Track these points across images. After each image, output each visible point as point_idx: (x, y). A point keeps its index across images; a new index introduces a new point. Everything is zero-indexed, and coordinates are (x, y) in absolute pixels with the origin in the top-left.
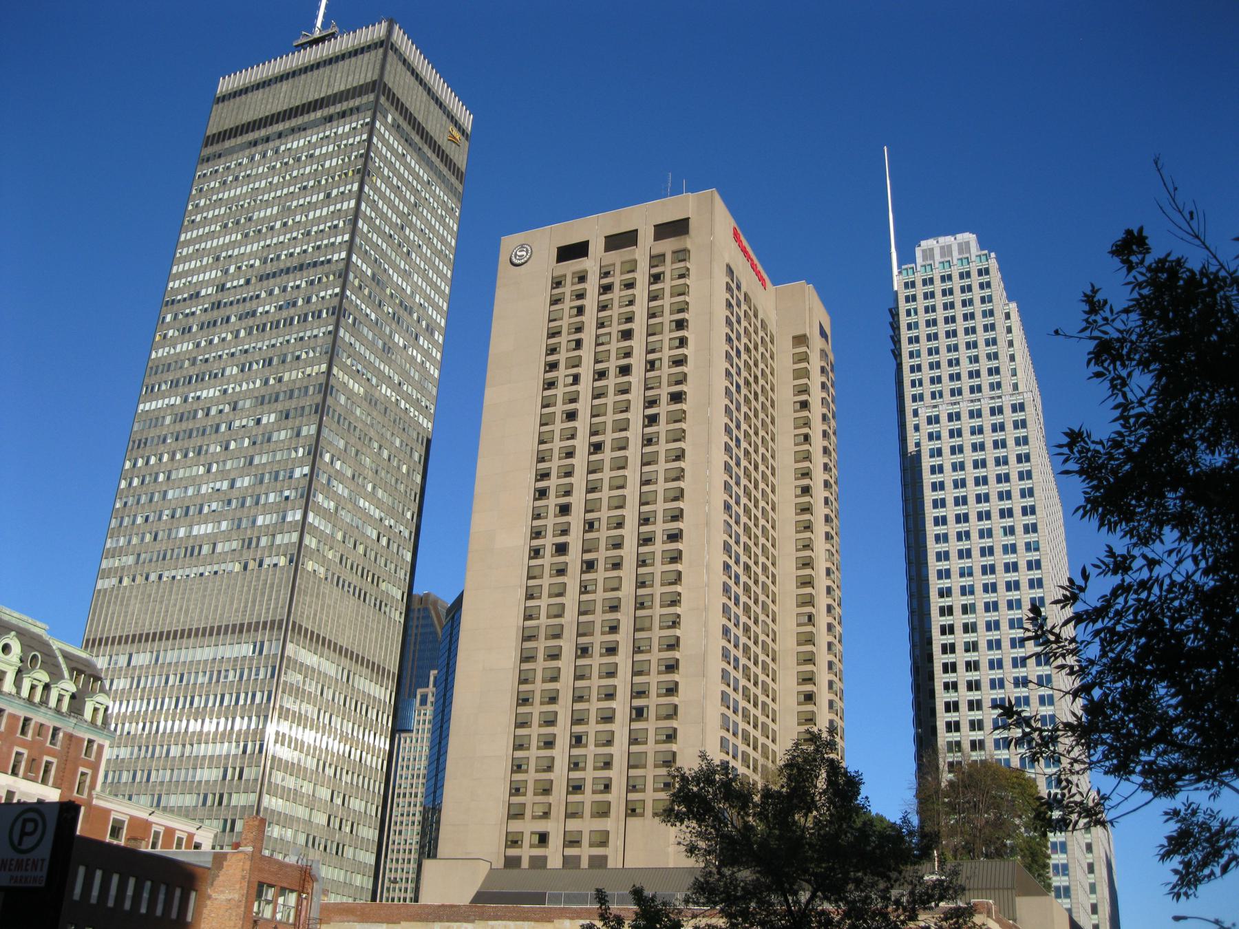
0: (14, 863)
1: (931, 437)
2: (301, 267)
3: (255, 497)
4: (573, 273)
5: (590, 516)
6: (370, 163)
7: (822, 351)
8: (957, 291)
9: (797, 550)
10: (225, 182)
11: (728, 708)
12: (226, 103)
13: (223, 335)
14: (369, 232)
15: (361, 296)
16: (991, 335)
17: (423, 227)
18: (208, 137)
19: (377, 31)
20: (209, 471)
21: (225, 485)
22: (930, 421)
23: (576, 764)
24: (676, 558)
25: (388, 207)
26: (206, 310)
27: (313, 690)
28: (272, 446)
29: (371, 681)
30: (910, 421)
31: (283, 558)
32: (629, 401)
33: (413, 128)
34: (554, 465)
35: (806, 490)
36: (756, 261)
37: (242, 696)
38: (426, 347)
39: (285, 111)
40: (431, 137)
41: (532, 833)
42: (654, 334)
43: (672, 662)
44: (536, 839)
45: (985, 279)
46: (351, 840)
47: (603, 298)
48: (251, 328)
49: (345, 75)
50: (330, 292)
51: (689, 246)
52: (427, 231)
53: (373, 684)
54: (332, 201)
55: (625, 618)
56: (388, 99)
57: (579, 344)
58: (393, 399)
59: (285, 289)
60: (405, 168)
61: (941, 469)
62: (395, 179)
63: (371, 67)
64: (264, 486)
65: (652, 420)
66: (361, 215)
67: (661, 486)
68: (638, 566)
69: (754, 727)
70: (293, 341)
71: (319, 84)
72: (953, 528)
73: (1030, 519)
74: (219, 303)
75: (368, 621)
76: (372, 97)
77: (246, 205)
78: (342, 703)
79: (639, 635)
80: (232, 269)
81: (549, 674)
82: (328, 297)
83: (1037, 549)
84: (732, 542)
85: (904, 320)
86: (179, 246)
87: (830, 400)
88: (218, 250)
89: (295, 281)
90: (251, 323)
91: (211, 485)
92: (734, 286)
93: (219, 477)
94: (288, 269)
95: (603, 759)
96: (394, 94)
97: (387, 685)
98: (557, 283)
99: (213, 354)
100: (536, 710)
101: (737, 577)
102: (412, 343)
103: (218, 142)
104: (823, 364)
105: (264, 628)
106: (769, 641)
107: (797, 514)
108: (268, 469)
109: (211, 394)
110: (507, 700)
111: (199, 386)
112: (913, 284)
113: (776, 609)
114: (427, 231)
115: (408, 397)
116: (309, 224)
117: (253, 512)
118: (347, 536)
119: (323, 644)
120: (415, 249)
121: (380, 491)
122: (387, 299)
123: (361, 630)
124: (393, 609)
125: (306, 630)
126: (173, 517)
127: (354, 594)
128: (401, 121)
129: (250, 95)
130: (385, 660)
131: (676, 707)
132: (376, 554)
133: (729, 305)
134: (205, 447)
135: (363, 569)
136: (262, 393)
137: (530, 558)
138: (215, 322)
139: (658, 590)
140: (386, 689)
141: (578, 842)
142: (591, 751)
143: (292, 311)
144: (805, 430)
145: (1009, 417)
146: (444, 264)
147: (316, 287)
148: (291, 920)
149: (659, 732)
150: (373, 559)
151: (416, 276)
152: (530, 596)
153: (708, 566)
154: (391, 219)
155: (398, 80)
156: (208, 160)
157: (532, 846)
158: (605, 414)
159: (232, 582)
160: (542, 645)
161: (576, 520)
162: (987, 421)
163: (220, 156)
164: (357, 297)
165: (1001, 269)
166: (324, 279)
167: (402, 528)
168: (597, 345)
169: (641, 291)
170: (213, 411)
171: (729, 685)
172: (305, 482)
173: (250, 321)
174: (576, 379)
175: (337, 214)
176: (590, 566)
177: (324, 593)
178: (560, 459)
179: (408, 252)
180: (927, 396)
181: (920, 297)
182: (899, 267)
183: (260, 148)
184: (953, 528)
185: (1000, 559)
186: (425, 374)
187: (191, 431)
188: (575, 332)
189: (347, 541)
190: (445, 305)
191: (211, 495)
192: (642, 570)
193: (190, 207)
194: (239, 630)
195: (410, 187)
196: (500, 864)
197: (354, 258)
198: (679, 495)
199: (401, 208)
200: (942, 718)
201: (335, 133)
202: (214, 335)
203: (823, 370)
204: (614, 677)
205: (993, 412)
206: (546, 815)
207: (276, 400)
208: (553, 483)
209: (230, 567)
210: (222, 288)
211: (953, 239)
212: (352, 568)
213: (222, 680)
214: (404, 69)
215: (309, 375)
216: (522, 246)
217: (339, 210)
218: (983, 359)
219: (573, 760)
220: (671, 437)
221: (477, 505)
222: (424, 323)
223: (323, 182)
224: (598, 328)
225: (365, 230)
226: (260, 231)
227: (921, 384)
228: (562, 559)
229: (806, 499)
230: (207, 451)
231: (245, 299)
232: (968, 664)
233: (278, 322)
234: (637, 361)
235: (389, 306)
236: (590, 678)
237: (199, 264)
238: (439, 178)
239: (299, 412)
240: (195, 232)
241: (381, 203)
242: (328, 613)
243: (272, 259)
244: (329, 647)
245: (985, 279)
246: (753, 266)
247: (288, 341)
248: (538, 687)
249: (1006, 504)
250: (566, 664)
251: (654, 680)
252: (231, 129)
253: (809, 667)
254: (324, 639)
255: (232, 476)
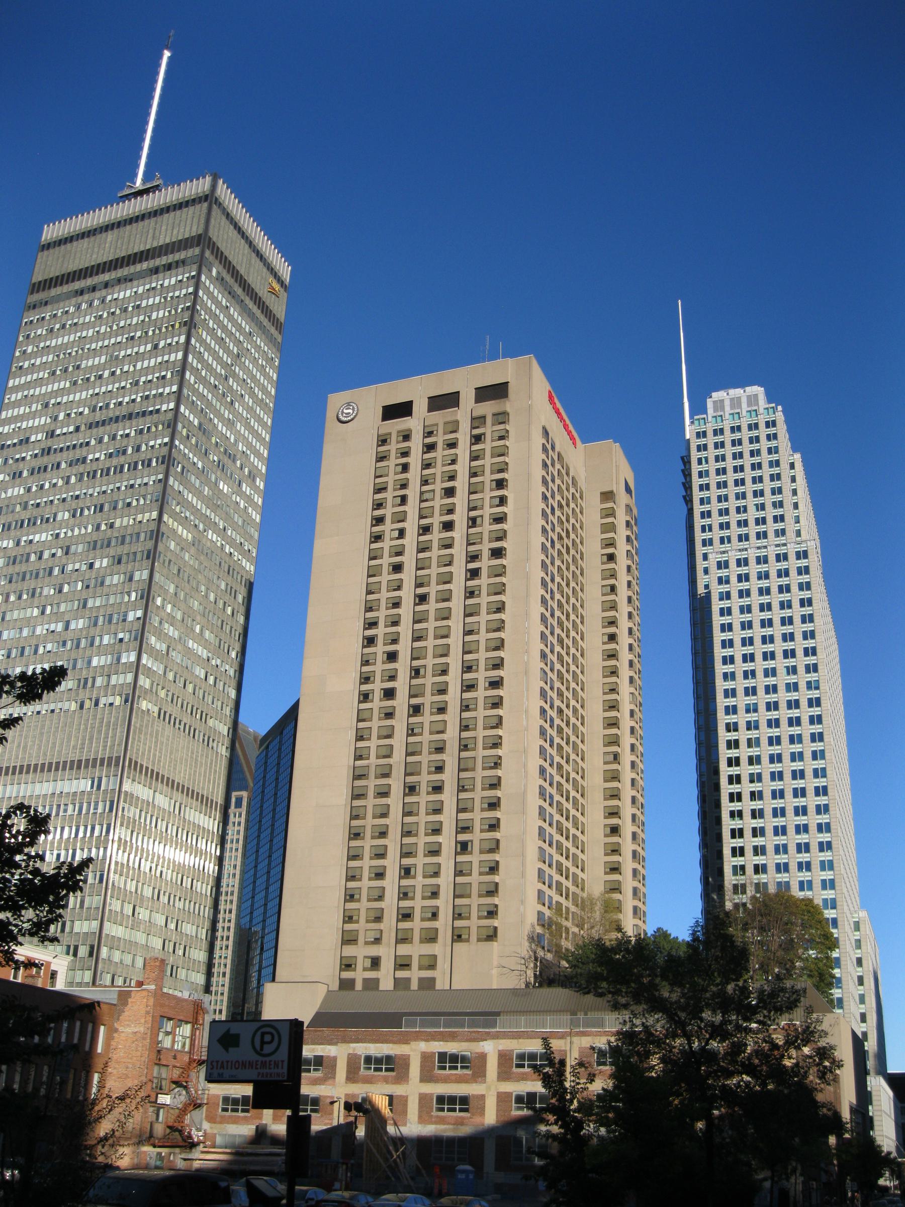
0: (259, 1063)
1: (720, 581)
2: (130, 416)
3: (89, 639)
4: (399, 432)
5: (416, 663)
6: (196, 315)
7: (627, 506)
8: (746, 441)
9: (604, 693)
10: (52, 330)
11: (545, 841)
12: (51, 251)
13: (54, 481)
14: (196, 383)
15: (189, 445)
16: (776, 484)
17: (245, 377)
18: (34, 284)
19: (202, 185)
20: (43, 613)
21: (60, 627)
22: (719, 565)
23: (405, 894)
24: (497, 704)
25: (214, 359)
26: (36, 455)
27: (131, 815)
28: (106, 590)
29: (201, 812)
30: (700, 564)
31: (118, 698)
32: (452, 555)
33: (236, 281)
34: (382, 614)
35: (612, 638)
36: (568, 422)
37: (82, 829)
38: (248, 493)
39: (111, 261)
40: (253, 289)
41: (365, 957)
42: (475, 493)
43: (494, 801)
44: (368, 963)
45: (772, 431)
46: (184, 962)
47: (426, 456)
48: (82, 474)
49: (170, 227)
50: (159, 441)
51: (508, 410)
52: (249, 381)
53: (202, 815)
54: (160, 353)
55: (450, 759)
56: (212, 253)
57: (404, 500)
58: (219, 544)
59: (114, 438)
60: (229, 320)
61: (729, 611)
62: (219, 331)
63: (196, 220)
64: (99, 628)
65: (474, 574)
66: (188, 367)
67: (483, 636)
68: (462, 711)
69: (550, 845)
70: (123, 488)
71: (145, 236)
72: (740, 667)
73: (811, 660)
74: (49, 449)
75: (197, 756)
76: (197, 251)
77: (74, 354)
78: (174, 834)
79: (463, 775)
80: (61, 416)
81: (379, 811)
82: (157, 446)
83: (817, 688)
84: (547, 688)
85: (695, 468)
86: (8, 391)
87: (634, 552)
88: (47, 397)
89: (124, 430)
90: (81, 470)
91: (46, 626)
92: (549, 447)
93: (54, 618)
94: (117, 417)
95: (430, 889)
96: (218, 248)
97: (215, 816)
98: (383, 441)
99: (45, 500)
100: (367, 844)
101: (552, 720)
102: (235, 489)
103: (44, 290)
104: (628, 518)
105: (102, 764)
106: (579, 778)
107: (604, 660)
108: (102, 612)
109: (43, 539)
110: (339, 835)
111: (32, 530)
112: (704, 434)
113: (585, 748)
114: (249, 381)
115: (232, 542)
116: (137, 374)
117: (88, 653)
118: (178, 676)
119: (157, 779)
120: (238, 398)
121: (207, 632)
122: (213, 447)
123: (191, 765)
124: (220, 744)
125: (142, 766)
126: (8, 657)
127: (184, 731)
128: (224, 274)
129: (75, 243)
130: (213, 792)
131: (498, 841)
132: (204, 692)
133: (545, 465)
134: (38, 590)
135: (193, 706)
136: (95, 538)
137: (360, 702)
138: (46, 468)
139: (481, 733)
140: (215, 819)
141: (408, 965)
142: (419, 881)
143: (122, 459)
144: (612, 581)
145: (793, 564)
146: (265, 413)
147: (146, 436)
148: (187, 1049)
149: (483, 864)
150: (201, 697)
151: (239, 424)
152: (360, 738)
153: (527, 711)
154: (216, 370)
155: (222, 234)
156: (34, 307)
157: (365, 969)
158: (429, 567)
159: (69, 720)
160: (372, 783)
161: (403, 666)
162: (773, 567)
163: (46, 303)
164: (185, 447)
165: (787, 421)
166: (153, 429)
167: (227, 667)
168: (422, 501)
169: (463, 451)
170: (46, 555)
171: (545, 821)
172: (138, 626)
173: (81, 468)
174: (402, 533)
175: (164, 365)
176: (416, 710)
177: (157, 731)
178: (387, 609)
179: (232, 402)
180: (716, 541)
181: (711, 446)
182: (691, 417)
183: (86, 297)
184: (740, 667)
185: (783, 696)
186: (248, 520)
187: (24, 574)
188: (401, 489)
189: (177, 681)
190: (266, 452)
191: (46, 636)
192: (466, 715)
193: (17, 354)
194: (77, 766)
195: (233, 338)
196: (335, 986)
197: (182, 408)
198: (500, 645)
199: (225, 359)
200: (728, 843)
201: (161, 285)
202: (45, 480)
203: (628, 524)
204: (440, 813)
205: (778, 558)
206: (377, 941)
207: (108, 545)
208: (380, 631)
209: (66, 705)
210: (51, 434)
211: (742, 391)
212: (182, 707)
213: (61, 813)
214: (228, 223)
215: (140, 522)
216: (349, 404)
217: (167, 361)
218: (769, 506)
219: (402, 890)
220: (492, 591)
221: (309, 650)
222: (246, 470)
223: (150, 333)
224: (422, 485)
225: (192, 381)
226: (88, 379)
227: (710, 530)
228: (389, 703)
229: (612, 646)
230: (41, 593)
231: (74, 446)
232: (753, 794)
233: (108, 469)
234: (460, 518)
235: (214, 454)
236: (417, 815)
237: (27, 410)
238: (260, 328)
239: (131, 557)
240: (23, 379)
241: (206, 354)
242: (161, 749)
243: (101, 407)
244: (162, 782)
245: (772, 431)
246: (566, 427)
247: (119, 488)
248: (369, 822)
249: (789, 645)
250: (395, 801)
251: (477, 816)
252: (57, 277)
253: (614, 802)
254: (158, 774)
255: (66, 618)
